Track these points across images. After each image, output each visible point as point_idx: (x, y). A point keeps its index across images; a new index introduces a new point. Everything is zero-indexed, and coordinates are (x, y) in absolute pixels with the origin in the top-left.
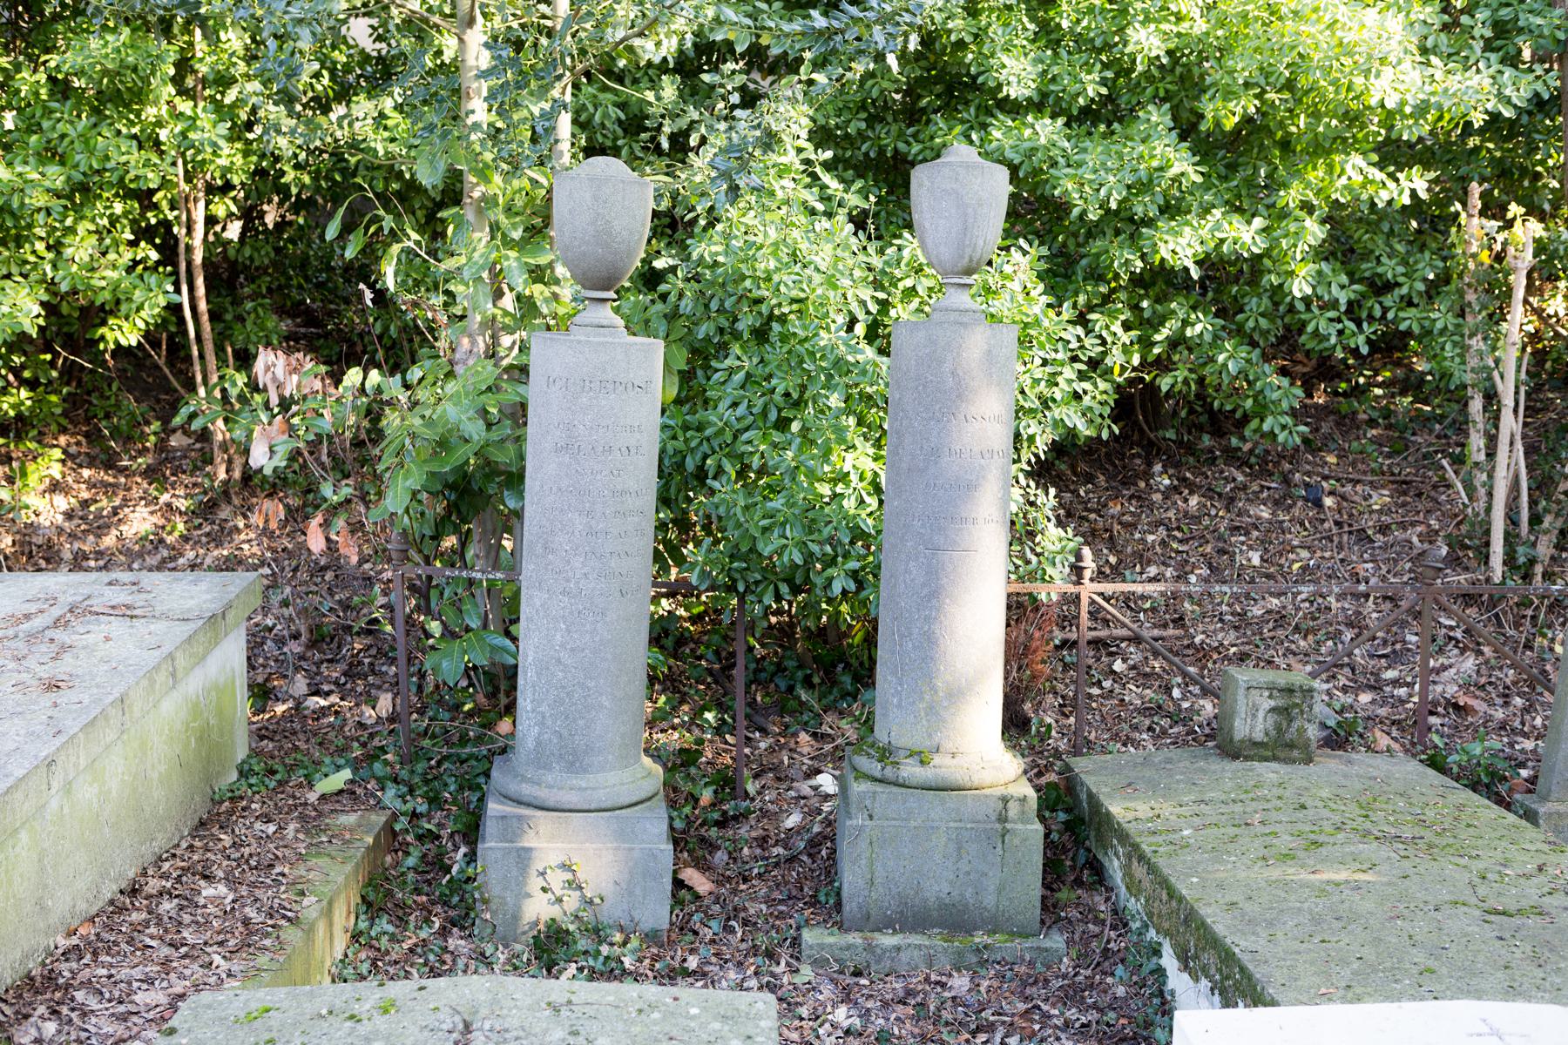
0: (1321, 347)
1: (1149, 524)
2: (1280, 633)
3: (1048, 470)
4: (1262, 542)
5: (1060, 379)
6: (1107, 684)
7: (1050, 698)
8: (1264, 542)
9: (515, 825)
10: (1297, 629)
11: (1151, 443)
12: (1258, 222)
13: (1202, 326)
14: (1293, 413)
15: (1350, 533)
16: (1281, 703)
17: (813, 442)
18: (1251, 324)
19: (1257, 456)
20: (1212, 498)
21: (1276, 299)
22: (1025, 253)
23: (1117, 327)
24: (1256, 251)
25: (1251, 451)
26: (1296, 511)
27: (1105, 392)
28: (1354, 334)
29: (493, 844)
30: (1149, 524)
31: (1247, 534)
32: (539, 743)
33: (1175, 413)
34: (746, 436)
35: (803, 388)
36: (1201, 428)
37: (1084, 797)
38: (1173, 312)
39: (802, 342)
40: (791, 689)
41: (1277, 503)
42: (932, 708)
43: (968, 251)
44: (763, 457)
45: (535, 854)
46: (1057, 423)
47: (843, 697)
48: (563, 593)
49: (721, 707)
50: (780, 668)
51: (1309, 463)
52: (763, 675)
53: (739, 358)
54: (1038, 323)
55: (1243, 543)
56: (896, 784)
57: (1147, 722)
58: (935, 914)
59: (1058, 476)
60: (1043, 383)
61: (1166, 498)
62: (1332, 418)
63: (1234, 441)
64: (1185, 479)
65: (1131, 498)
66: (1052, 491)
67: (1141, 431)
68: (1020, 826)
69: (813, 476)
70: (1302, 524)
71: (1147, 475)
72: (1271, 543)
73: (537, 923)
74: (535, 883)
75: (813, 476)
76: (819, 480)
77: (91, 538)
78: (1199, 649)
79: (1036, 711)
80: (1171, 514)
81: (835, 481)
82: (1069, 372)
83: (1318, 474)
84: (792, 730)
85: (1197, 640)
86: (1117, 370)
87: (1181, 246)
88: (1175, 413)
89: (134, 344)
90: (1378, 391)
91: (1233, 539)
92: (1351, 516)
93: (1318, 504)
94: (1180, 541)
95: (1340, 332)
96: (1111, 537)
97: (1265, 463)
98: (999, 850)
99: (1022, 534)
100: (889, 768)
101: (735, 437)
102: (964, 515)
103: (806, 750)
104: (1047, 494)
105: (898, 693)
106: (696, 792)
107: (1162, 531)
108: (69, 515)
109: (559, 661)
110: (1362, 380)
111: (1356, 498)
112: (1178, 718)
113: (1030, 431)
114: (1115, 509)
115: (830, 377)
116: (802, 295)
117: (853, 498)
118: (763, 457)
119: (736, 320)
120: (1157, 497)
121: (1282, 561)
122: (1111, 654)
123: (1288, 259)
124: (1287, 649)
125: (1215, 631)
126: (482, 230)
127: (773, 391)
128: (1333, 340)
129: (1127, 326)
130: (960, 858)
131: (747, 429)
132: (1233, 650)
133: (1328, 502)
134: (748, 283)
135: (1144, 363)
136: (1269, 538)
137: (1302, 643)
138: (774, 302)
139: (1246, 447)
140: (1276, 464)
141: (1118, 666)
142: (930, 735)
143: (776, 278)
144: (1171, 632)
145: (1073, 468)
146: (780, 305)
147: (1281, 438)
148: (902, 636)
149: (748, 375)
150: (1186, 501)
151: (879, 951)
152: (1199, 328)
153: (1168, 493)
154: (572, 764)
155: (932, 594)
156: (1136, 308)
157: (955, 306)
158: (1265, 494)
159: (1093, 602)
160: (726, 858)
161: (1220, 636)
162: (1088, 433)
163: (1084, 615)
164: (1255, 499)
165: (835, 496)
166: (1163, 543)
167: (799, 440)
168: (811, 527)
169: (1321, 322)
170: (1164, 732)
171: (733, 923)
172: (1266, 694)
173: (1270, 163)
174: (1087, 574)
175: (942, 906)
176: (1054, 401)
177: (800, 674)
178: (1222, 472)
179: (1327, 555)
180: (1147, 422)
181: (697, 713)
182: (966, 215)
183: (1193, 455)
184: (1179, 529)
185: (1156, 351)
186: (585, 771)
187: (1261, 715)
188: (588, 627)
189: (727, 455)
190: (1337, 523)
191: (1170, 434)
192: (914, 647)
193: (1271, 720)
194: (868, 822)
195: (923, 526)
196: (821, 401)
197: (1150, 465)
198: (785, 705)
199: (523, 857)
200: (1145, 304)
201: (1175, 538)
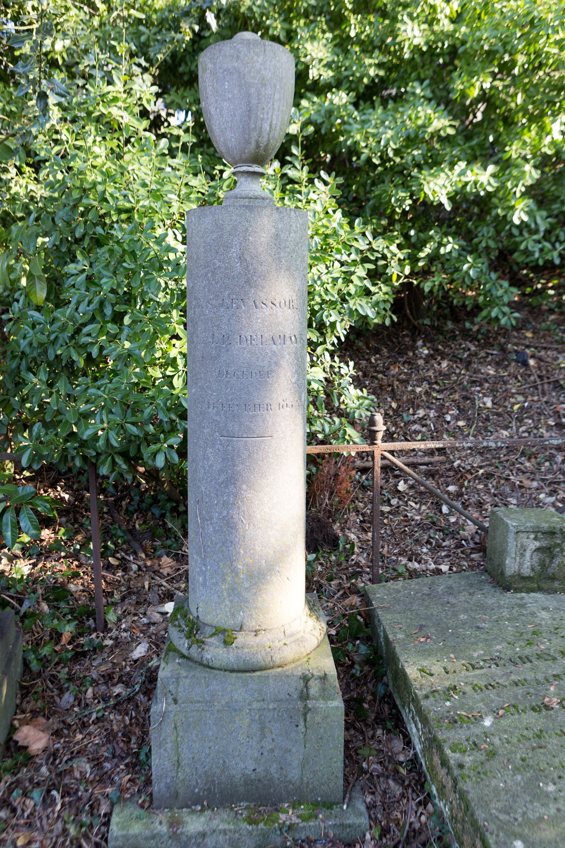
0: (528, 260)
1: (417, 380)
2: (512, 457)
3: (351, 346)
4: (492, 391)
5: (354, 278)
6: (394, 502)
7: (353, 516)
8: (493, 391)
10: (523, 454)
11: (415, 328)
12: (491, 168)
13: (450, 246)
14: (510, 304)
15: (549, 383)
16: (545, 543)
18: (483, 244)
19: (483, 334)
20: (455, 362)
21: (499, 228)
22: (326, 183)
23: (394, 248)
24: (490, 189)
25: (478, 331)
26: (511, 369)
27: (387, 293)
28: (550, 251)
30: (417, 380)
31: (481, 385)
33: (429, 308)
34: (85, 330)
36: (445, 317)
37: (382, 634)
38: (431, 237)
40: (163, 516)
41: (498, 364)
42: (233, 589)
43: (254, 135)
46: (351, 313)
51: (516, 337)
54: (335, 233)
55: (479, 392)
56: (201, 664)
57: (426, 537)
58: (242, 789)
59: (357, 350)
60: (340, 281)
61: (427, 362)
62: (526, 309)
63: (467, 325)
64: (437, 350)
65: (404, 363)
66: (351, 364)
67: (409, 320)
68: (321, 704)
70: (516, 378)
71: (414, 348)
72: (497, 391)
78: (457, 471)
79: (342, 530)
80: (431, 373)
82: (361, 271)
83: (523, 345)
85: (455, 464)
86: (394, 278)
87: (438, 187)
88: (429, 308)
90: (551, 292)
91: (473, 389)
92: (548, 371)
93: (525, 364)
94: (438, 392)
95: (541, 250)
96: (393, 390)
97: (492, 338)
98: (301, 728)
99: (325, 400)
100: (195, 647)
102: (257, 402)
103: (165, 572)
104: (348, 366)
105: (203, 573)
107: (425, 385)
110: (539, 286)
111: (548, 360)
112: (450, 532)
113: (332, 319)
114: (394, 371)
116: (128, 205)
120: (421, 362)
121: (507, 404)
122: (396, 477)
123: (509, 197)
124: (519, 469)
125: (466, 456)
128: (537, 255)
129: (400, 247)
130: (263, 736)
132: (481, 471)
133: (532, 362)
135: (413, 274)
136: (496, 388)
137: (528, 464)
139: (475, 328)
140: (495, 339)
141: (402, 486)
142: (233, 615)
144: (437, 458)
145: (367, 344)
147: (503, 321)
148: (203, 520)
150: (439, 364)
151: (184, 838)
152: (449, 248)
153: (428, 358)
155: (232, 480)
156: (406, 236)
157: (243, 194)
158: (489, 359)
159: (384, 458)
160: (72, 700)
161: (470, 460)
162: (376, 321)
163: (378, 469)
164: (483, 362)
166: (427, 393)
169: (528, 243)
170: (439, 547)
171: (54, 793)
172: (532, 536)
173: (496, 131)
174: (380, 435)
175: (248, 782)
176: (349, 294)
177: (169, 505)
178: (460, 345)
179: (536, 398)
180: (412, 314)
182: (249, 95)
183: (441, 334)
184: (436, 383)
185: (421, 264)
187: (528, 554)
190: (539, 377)
191: (427, 322)
192: (215, 531)
193: (536, 559)
194: (172, 707)
195: (218, 413)
197: (415, 341)
200: (412, 233)
201: (434, 389)
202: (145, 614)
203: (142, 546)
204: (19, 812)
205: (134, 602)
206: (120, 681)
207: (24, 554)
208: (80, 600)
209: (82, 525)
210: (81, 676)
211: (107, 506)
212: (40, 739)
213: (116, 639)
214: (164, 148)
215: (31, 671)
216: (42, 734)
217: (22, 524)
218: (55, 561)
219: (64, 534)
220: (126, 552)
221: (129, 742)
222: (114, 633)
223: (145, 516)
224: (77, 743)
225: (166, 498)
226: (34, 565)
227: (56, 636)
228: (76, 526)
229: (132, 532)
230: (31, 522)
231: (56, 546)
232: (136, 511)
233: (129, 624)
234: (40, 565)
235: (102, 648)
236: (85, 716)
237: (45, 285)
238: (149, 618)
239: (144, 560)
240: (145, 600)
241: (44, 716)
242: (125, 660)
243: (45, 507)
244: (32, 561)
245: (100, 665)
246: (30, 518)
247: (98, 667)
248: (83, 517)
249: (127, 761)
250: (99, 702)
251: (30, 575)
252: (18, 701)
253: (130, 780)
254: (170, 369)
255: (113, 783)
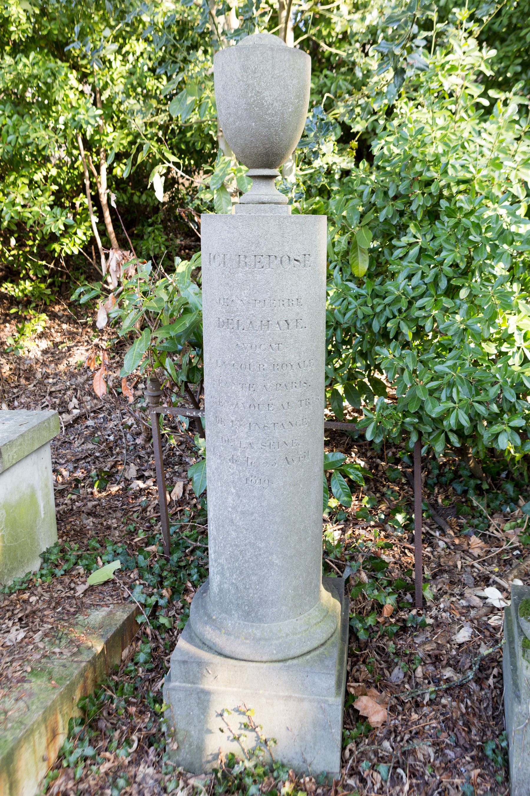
9: (196, 669)
17: (480, 308)
29: (177, 684)
32: (221, 590)
34: (419, 303)
35: (470, 259)
39: (468, 214)
40: (465, 492)
44: (434, 320)
45: (213, 698)
47: (507, 503)
48: (232, 460)
49: (409, 507)
50: (457, 476)
52: (444, 479)
53: (415, 237)
69: (479, 338)
73: (216, 756)
74: (214, 723)
75: (479, 338)
76: (485, 341)
77: (53, 365)
81: (501, 341)
84: (466, 532)
89: (76, 252)
101: (410, 303)
103: (476, 552)
106: (381, 600)
108: (45, 352)
109: (232, 521)
115: (495, 247)
116: (468, 176)
117: (517, 356)
118: (434, 320)
119: (410, 203)
126: (230, 155)
127: (442, 263)
131: (422, 296)
134: (418, 167)
138: (443, 183)
143: (443, 160)
146: (448, 186)
149: (422, 250)
154: (248, 614)
160: (401, 676)
165: (501, 354)
167: (465, 306)
168: (478, 387)
171: (400, 771)
177: (472, 482)
181: (390, 515)
186: (261, 620)
188: (255, 493)
189: (405, 319)
196: (486, 271)
198: (460, 508)
199: (203, 698)
202: (462, 595)
203: (447, 522)
204: (369, 784)
205: (447, 581)
206: (448, 665)
207: (331, 519)
208: (394, 572)
209: (383, 495)
210: (408, 652)
211: (405, 476)
212: (377, 712)
213: (436, 618)
214: (512, 115)
215: (357, 639)
216: (379, 707)
217: (334, 490)
218: (363, 528)
219: (368, 502)
220: (429, 526)
221: (470, 731)
222: (434, 612)
223: (446, 491)
224: (415, 723)
225: (469, 474)
226: (344, 531)
227: (379, 607)
228: (378, 495)
229: (434, 505)
230: (343, 489)
231: (366, 514)
232: (435, 484)
233: (448, 604)
234: (350, 532)
235: (423, 625)
236: (418, 696)
237: (367, 257)
238: (468, 601)
239: (452, 537)
240: (459, 581)
241: (376, 687)
242: (448, 642)
243: (357, 475)
244: (340, 527)
245: (424, 643)
246: (341, 485)
247: (423, 645)
248: (384, 486)
249: (473, 753)
250: (429, 683)
251: (340, 540)
252: (349, 668)
253: (479, 775)
254: (506, 345)
255: (460, 774)
